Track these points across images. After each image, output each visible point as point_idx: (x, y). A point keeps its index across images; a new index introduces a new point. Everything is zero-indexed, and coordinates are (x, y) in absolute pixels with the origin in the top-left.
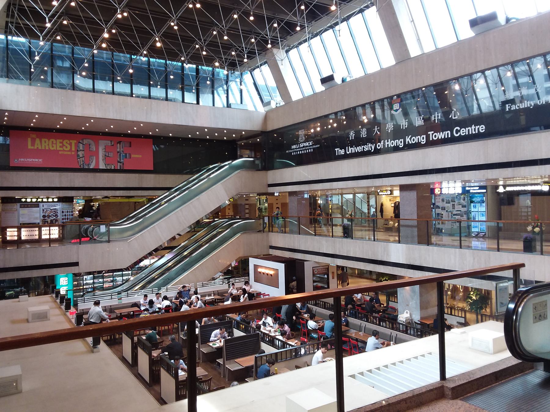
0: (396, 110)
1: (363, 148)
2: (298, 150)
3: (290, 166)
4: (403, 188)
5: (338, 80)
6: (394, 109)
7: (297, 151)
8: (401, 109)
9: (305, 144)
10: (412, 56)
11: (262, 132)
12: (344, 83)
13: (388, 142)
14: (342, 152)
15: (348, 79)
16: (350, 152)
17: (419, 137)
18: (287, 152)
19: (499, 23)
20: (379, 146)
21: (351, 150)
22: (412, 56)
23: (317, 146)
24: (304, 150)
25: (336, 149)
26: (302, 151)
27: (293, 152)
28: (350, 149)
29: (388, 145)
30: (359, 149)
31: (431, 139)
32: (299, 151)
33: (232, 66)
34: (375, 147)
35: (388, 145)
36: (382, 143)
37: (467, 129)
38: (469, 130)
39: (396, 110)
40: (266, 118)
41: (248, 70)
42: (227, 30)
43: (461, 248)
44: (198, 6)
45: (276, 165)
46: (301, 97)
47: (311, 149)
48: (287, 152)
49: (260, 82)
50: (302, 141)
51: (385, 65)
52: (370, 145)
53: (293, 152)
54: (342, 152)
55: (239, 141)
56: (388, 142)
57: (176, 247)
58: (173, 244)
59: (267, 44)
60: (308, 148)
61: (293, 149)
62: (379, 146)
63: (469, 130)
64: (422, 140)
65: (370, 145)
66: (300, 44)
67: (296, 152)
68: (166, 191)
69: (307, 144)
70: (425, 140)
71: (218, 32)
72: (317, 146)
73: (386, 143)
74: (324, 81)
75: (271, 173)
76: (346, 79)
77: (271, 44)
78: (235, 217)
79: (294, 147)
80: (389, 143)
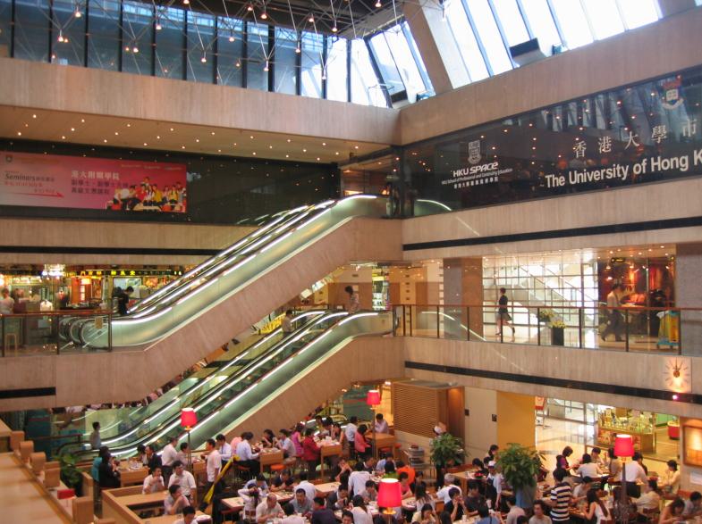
0: (673, 102)
1: (605, 174)
2: (465, 178)
3: (442, 211)
4: (448, 263)
5: (545, 49)
6: (669, 99)
7: (465, 182)
8: (682, 100)
9: (481, 168)
10: (455, 86)
11: (392, 146)
12: (556, 56)
13: (656, 161)
14: (560, 181)
15: (563, 50)
16: (577, 180)
17: (676, 159)
18: (444, 183)
19: (542, 54)
20: (637, 169)
21: (579, 178)
22: (455, 86)
23: (507, 171)
24: (479, 179)
25: (548, 177)
26: (474, 180)
27: (457, 183)
28: (577, 176)
29: (656, 167)
30: (596, 176)
31: (549, 186)
32: (470, 181)
33: (324, 27)
34: (630, 171)
35: (656, 167)
36: (644, 164)
37: (672, 160)
38: (675, 161)
39: (673, 102)
40: (401, 120)
41: (359, 36)
42: (268, 5)
43: (627, 351)
44: (136, 50)
45: (417, 210)
46: (484, 75)
47: (494, 176)
48: (444, 183)
49: (383, 60)
50: (474, 162)
51: (497, 71)
52: (618, 168)
53: (457, 183)
54: (560, 181)
55: (344, 164)
56: (656, 161)
57: (226, 363)
58: (224, 357)
59: (333, 27)
60: (488, 174)
61: (457, 177)
62: (637, 169)
63: (675, 161)
64: (683, 166)
65: (618, 168)
66: (386, 28)
67: (461, 182)
68: (208, 257)
69: (486, 167)
70: (687, 164)
71: (255, 8)
72: (507, 171)
73: (653, 164)
74: (516, 52)
75: (409, 224)
76: (559, 48)
77: (337, 28)
78: (335, 306)
79: (459, 173)
80: (658, 163)
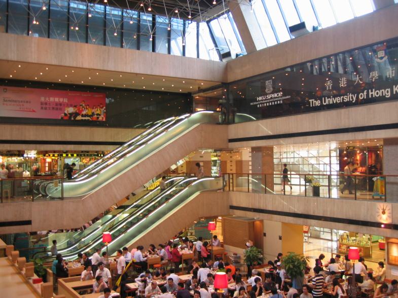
0: (382, 58)
1: (343, 99)
2: (264, 102)
3: (251, 120)
4: (254, 149)
5: (309, 28)
6: (379, 56)
7: (264, 103)
8: (386, 57)
9: (273, 96)
10: (258, 49)
11: (222, 83)
12: (315, 32)
13: (372, 91)
14: (318, 103)
15: (319, 28)
16: (327, 102)
17: (383, 90)
18: (252, 104)
19: (307, 31)
20: (361, 96)
21: (328, 101)
22: (258, 49)
23: (287, 97)
24: (272, 102)
25: (311, 101)
26: (269, 102)
27: (259, 104)
28: (327, 100)
29: (372, 95)
30: (338, 100)
31: (311, 106)
32: (266, 103)
34: (357, 97)
35: (372, 95)
36: (365, 93)
37: (381, 91)
38: (382, 92)
39: (382, 58)
40: (227, 68)
41: (204, 21)
42: (152, 3)
43: (356, 199)
44: (77, 29)
45: (236, 120)
46: (274, 43)
47: (280, 100)
48: (252, 104)
49: (217, 34)
50: (269, 92)
51: (282, 40)
52: (351, 95)
53: (259, 104)
54: (318, 103)
55: (195, 93)
56: (372, 91)
57: (128, 206)
58: (127, 203)
59: (189, 15)
60: (276, 99)
61: (259, 101)
62: (361, 96)
63: (382, 92)
64: (387, 94)
65: (351, 95)
66: (219, 16)
67: (262, 104)
68: (118, 146)
69: (276, 95)
70: (389, 93)
71: (145, 5)
72: (287, 97)
73: (370, 93)
74: (293, 29)
75: (232, 127)
76: (317, 27)
77: (191, 16)
78: (190, 174)
79: (260, 98)
80: (373, 93)
